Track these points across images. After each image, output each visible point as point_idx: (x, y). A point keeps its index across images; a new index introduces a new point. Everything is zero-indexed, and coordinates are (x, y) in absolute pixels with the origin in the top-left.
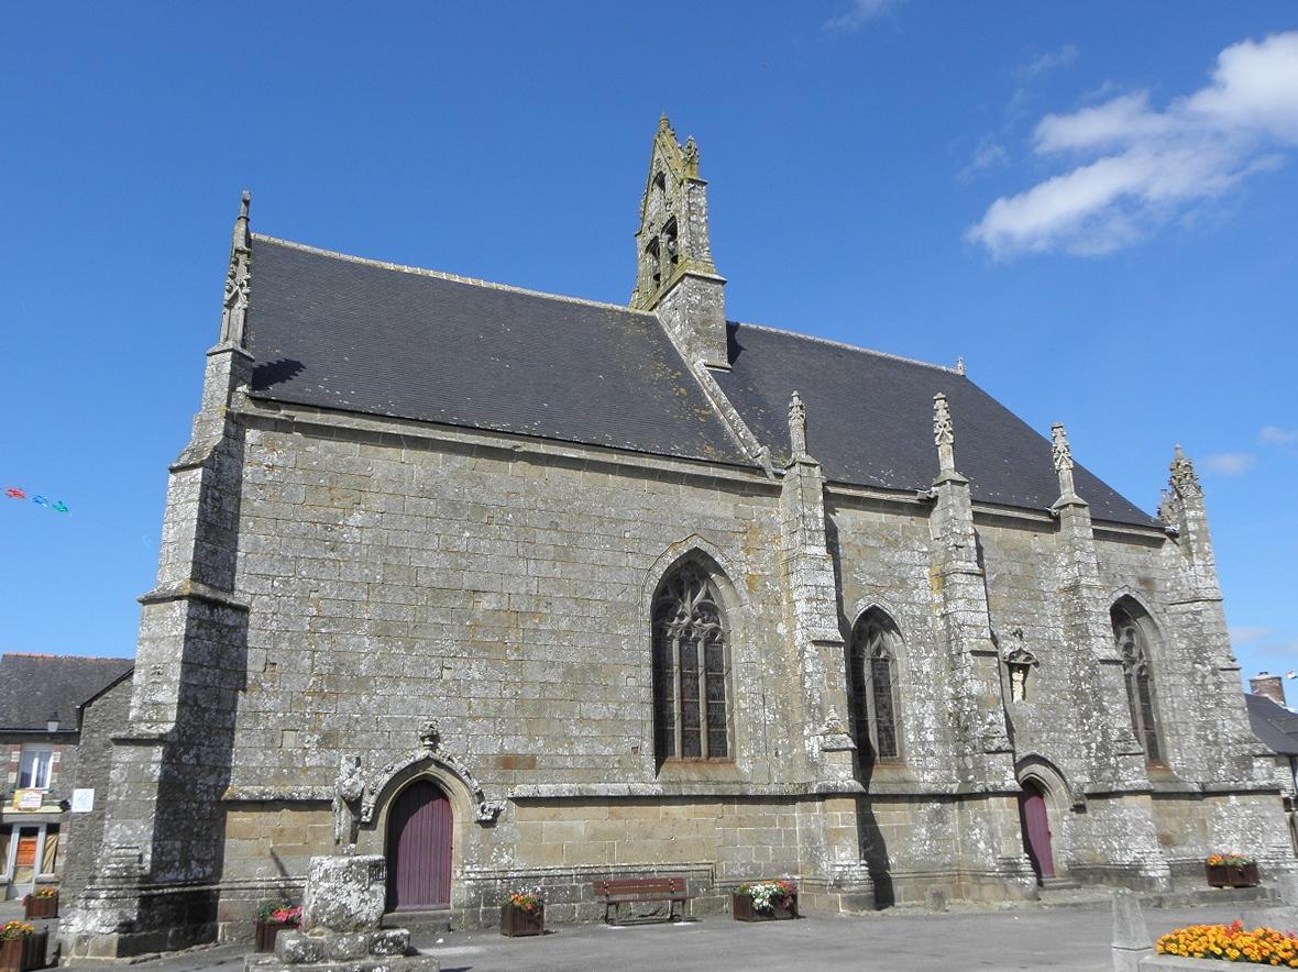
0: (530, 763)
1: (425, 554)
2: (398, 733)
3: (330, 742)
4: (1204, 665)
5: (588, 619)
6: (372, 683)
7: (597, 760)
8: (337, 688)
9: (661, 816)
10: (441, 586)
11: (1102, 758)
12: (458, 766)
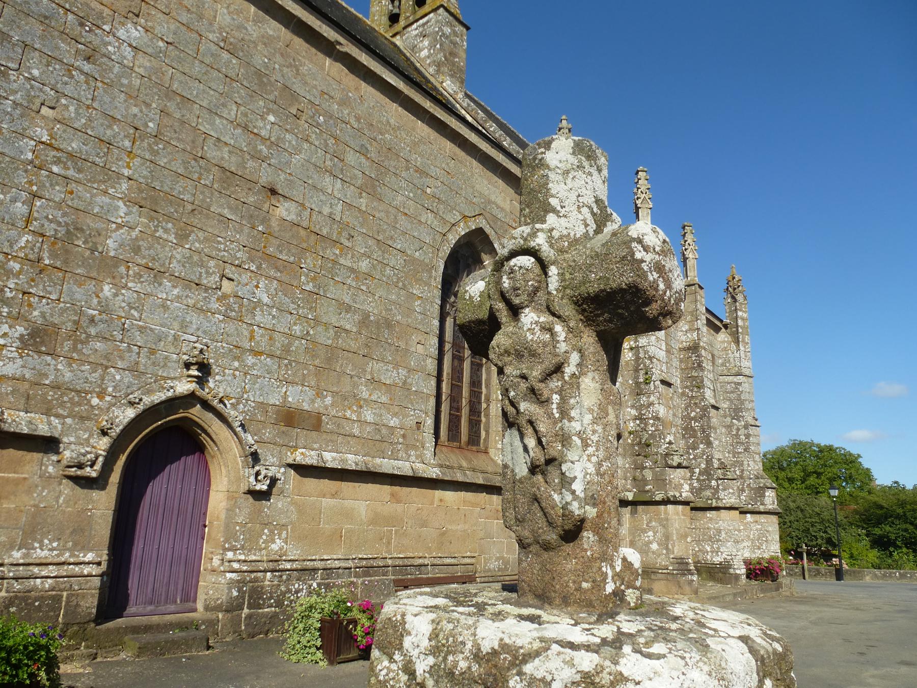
0: (315, 423)
1: (218, 121)
2: (152, 352)
3: (42, 343)
4: (739, 421)
5: (388, 268)
6: (122, 269)
7: (384, 431)
8: (66, 262)
9: (436, 503)
10: (233, 169)
11: (704, 480)
12: (230, 412)
